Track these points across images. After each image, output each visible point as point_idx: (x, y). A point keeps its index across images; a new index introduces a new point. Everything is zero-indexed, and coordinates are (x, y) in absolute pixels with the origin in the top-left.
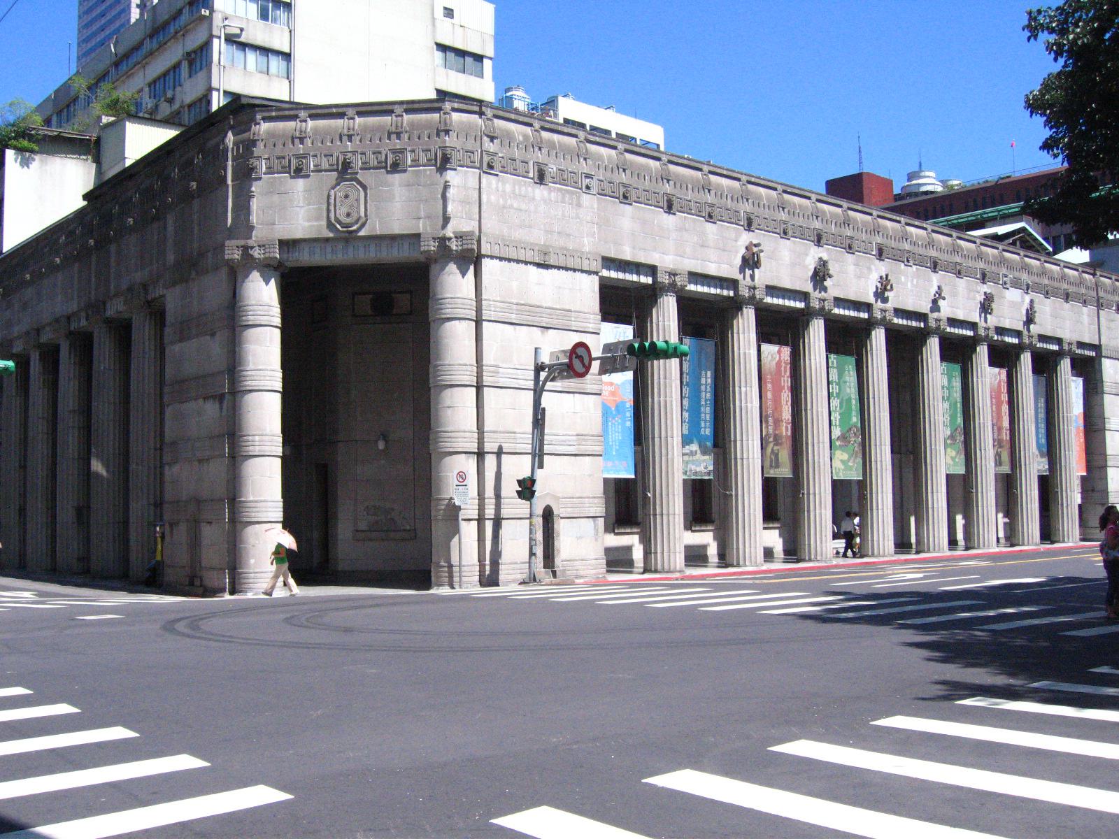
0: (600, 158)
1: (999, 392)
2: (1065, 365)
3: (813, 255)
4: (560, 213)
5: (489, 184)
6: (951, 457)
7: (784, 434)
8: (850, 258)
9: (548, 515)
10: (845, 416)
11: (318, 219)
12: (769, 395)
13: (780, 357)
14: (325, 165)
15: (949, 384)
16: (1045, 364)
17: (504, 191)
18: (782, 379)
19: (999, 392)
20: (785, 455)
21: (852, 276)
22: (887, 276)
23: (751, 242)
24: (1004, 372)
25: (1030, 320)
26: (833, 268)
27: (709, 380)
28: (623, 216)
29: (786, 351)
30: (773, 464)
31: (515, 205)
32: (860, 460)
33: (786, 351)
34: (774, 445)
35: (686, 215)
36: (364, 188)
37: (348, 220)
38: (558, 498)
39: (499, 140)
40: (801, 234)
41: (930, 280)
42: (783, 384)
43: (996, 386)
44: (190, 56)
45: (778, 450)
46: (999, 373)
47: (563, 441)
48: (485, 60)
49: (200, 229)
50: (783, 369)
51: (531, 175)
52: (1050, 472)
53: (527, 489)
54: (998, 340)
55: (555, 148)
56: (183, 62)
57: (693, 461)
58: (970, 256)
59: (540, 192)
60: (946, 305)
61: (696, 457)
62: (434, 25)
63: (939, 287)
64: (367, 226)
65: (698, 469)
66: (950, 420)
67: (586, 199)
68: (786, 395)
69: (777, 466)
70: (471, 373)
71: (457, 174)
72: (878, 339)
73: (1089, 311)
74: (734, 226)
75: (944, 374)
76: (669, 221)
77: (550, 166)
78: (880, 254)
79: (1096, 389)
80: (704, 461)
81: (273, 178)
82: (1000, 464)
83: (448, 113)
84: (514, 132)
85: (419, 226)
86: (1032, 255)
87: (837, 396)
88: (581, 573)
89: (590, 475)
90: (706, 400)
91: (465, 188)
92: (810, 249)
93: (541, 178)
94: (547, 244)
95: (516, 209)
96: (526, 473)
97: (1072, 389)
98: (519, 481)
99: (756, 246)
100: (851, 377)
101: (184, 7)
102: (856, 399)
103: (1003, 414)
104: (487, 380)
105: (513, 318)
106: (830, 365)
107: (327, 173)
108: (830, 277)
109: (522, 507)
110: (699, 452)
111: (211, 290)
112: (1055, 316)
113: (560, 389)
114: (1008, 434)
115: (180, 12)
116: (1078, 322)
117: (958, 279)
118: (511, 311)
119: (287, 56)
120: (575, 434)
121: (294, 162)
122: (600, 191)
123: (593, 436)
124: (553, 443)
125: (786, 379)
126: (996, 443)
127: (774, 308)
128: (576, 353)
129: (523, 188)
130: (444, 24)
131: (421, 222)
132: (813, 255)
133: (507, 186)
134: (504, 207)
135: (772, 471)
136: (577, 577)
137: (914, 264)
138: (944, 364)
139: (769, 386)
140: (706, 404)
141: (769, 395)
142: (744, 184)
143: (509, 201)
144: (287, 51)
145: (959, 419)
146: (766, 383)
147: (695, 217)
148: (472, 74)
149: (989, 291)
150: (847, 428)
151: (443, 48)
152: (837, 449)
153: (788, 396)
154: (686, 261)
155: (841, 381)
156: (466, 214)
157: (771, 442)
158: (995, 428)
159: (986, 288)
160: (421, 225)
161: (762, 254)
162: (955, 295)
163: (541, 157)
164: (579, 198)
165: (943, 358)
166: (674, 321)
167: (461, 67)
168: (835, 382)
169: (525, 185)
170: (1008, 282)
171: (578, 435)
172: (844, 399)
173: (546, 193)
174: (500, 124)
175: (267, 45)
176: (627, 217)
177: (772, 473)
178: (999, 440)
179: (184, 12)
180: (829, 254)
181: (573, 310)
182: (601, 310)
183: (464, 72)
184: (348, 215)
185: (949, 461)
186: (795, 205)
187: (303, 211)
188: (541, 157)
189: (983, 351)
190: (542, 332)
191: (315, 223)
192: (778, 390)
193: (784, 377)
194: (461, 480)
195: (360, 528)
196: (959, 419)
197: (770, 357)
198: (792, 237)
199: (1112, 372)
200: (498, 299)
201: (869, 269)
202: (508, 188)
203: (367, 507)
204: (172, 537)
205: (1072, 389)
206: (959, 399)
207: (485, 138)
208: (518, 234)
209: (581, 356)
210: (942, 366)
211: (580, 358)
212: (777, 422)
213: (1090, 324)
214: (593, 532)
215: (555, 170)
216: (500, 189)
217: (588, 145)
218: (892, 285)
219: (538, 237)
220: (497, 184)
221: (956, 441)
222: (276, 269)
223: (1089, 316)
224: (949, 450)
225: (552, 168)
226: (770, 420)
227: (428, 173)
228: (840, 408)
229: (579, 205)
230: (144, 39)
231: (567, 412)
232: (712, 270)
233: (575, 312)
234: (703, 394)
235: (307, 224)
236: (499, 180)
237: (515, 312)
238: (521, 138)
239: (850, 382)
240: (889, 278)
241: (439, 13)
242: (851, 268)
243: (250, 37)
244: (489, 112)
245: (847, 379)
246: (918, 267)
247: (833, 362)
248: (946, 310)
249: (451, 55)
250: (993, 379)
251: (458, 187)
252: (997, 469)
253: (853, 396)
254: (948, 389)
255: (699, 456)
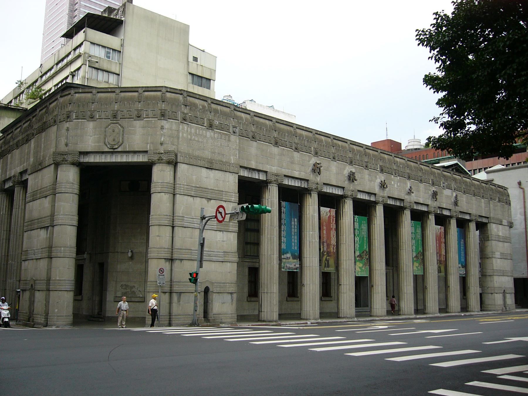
0: (241, 118)
1: (440, 237)
2: (472, 226)
3: (348, 169)
4: (219, 144)
5: (183, 129)
6: (416, 266)
7: (332, 251)
8: (366, 172)
9: (207, 291)
10: (361, 246)
11: (99, 142)
12: (325, 232)
13: (330, 214)
14: (103, 116)
15: (415, 231)
16: (462, 224)
17: (191, 132)
18: (331, 224)
19: (440, 237)
20: (332, 262)
21: (367, 180)
22: (384, 181)
23: (316, 162)
24: (443, 228)
25: (456, 204)
26: (357, 176)
27: (296, 223)
28: (252, 147)
29: (333, 211)
30: (326, 266)
31: (196, 139)
32: (368, 267)
33: (333, 211)
34: (327, 256)
35: (284, 148)
36: (122, 127)
37: (113, 143)
38: (213, 283)
39: (190, 107)
40: (342, 159)
41: (406, 184)
42: (331, 227)
43: (439, 235)
44: (73, 73)
45: (329, 259)
46: (441, 228)
47: (216, 255)
48: (211, 80)
49: (44, 146)
50: (331, 219)
51: (205, 125)
52: (466, 275)
53: (194, 278)
54: (440, 213)
55: (218, 113)
56: (70, 76)
57: (288, 262)
58: (426, 173)
59: (209, 133)
60: (414, 196)
61: (289, 260)
62: (188, 65)
63: (410, 187)
64: (122, 146)
65: (291, 266)
66: (415, 249)
67: (233, 138)
68: (333, 232)
69: (328, 267)
70: (170, 220)
71: (167, 123)
72: (379, 211)
73: (485, 201)
74: (308, 154)
75: (412, 226)
76: (275, 150)
77: (215, 121)
78: (382, 171)
79: (489, 238)
80: (294, 262)
81: (78, 121)
82: (440, 272)
83: (165, 94)
84: (197, 104)
85: (147, 147)
86: (457, 174)
87: (358, 236)
88: (223, 321)
89: (230, 272)
90: (295, 233)
91: (171, 129)
92: (346, 167)
93: (211, 126)
94: (212, 158)
95: (197, 141)
96: (194, 270)
97: (474, 234)
98: (191, 274)
99: (318, 164)
100: (365, 227)
101: (71, 51)
102: (366, 237)
103: (442, 248)
104: (176, 223)
105: (193, 193)
106: (355, 221)
107: (241, 137)
108: (356, 180)
109: (191, 287)
110: (291, 258)
111: (513, 146)
112: (468, 203)
113: (216, 229)
114: (444, 258)
115: (70, 53)
116: (479, 206)
117: (420, 184)
118: (192, 190)
119: (119, 75)
120: (223, 251)
121: (89, 113)
122: (241, 135)
123: (232, 253)
124: (211, 255)
125: (333, 224)
126: (438, 262)
127: (328, 194)
128: (219, 211)
129: (201, 131)
130: (193, 64)
131: (149, 145)
132: (348, 169)
133: (193, 129)
134: (190, 140)
135: (326, 269)
136: (221, 323)
137: (398, 176)
138: (412, 221)
139: (325, 228)
140: (295, 234)
141: (325, 232)
142: (314, 135)
143: (193, 137)
144: (118, 72)
145: (420, 248)
146: (323, 226)
147: (289, 149)
148: (205, 88)
149: (435, 190)
150: (362, 252)
151: (189, 73)
152: (357, 262)
153: (334, 233)
154: (283, 170)
155: (360, 229)
156: (171, 142)
157: (325, 255)
158: (438, 254)
159: (434, 189)
160: (148, 147)
161: (322, 168)
162: (418, 191)
163: (211, 116)
164: (229, 137)
165: (412, 219)
166: (276, 199)
167: (200, 84)
168: (357, 229)
169: (202, 129)
170: (445, 186)
171: (224, 252)
172: (361, 237)
173: (212, 134)
174: (191, 100)
175: (109, 70)
176: (253, 147)
177: (326, 270)
178: (440, 260)
179: (71, 53)
180: (355, 170)
181: (224, 191)
182: (239, 192)
183: (202, 87)
184: (114, 140)
185: (415, 268)
186: (339, 145)
187: (92, 138)
188: (211, 116)
189: (432, 218)
190: (208, 201)
191: (97, 144)
192: (329, 230)
193: (332, 224)
194: (161, 272)
195: (117, 296)
196: (420, 248)
197: (325, 214)
198: (337, 160)
199: (496, 230)
200: (186, 184)
201: (376, 177)
202: (193, 130)
203: (122, 285)
204: (23, 297)
205: (474, 234)
206: (420, 239)
207: (182, 106)
208: (197, 153)
209: (221, 212)
210: (411, 222)
211: (220, 213)
212: (328, 245)
213: (485, 207)
214: (230, 301)
215: (217, 123)
216: (189, 131)
217: (235, 112)
218: (387, 185)
219: (207, 154)
220: (188, 128)
221: (419, 258)
222: (77, 166)
223: (485, 203)
224: (415, 263)
225: (217, 122)
226: (325, 244)
227: (153, 121)
228: (359, 242)
229: (229, 140)
230: (54, 65)
231: (219, 241)
232: (296, 174)
233: (225, 192)
234: (293, 230)
235: (93, 144)
236: (189, 126)
237: (194, 190)
238: (201, 107)
239: (364, 229)
240: (385, 182)
241: (191, 59)
242: (367, 177)
243: (101, 66)
244: (209, 101)
245: (363, 227)
246: (400, 177)
247: (356, 219)
248: (413, 198)
249: (195, 78)
250: (438, 231)
251: (167, 129)
252: (439, 274)
253: (365, 236)
254: (414, 233)
255: (291, 260)
